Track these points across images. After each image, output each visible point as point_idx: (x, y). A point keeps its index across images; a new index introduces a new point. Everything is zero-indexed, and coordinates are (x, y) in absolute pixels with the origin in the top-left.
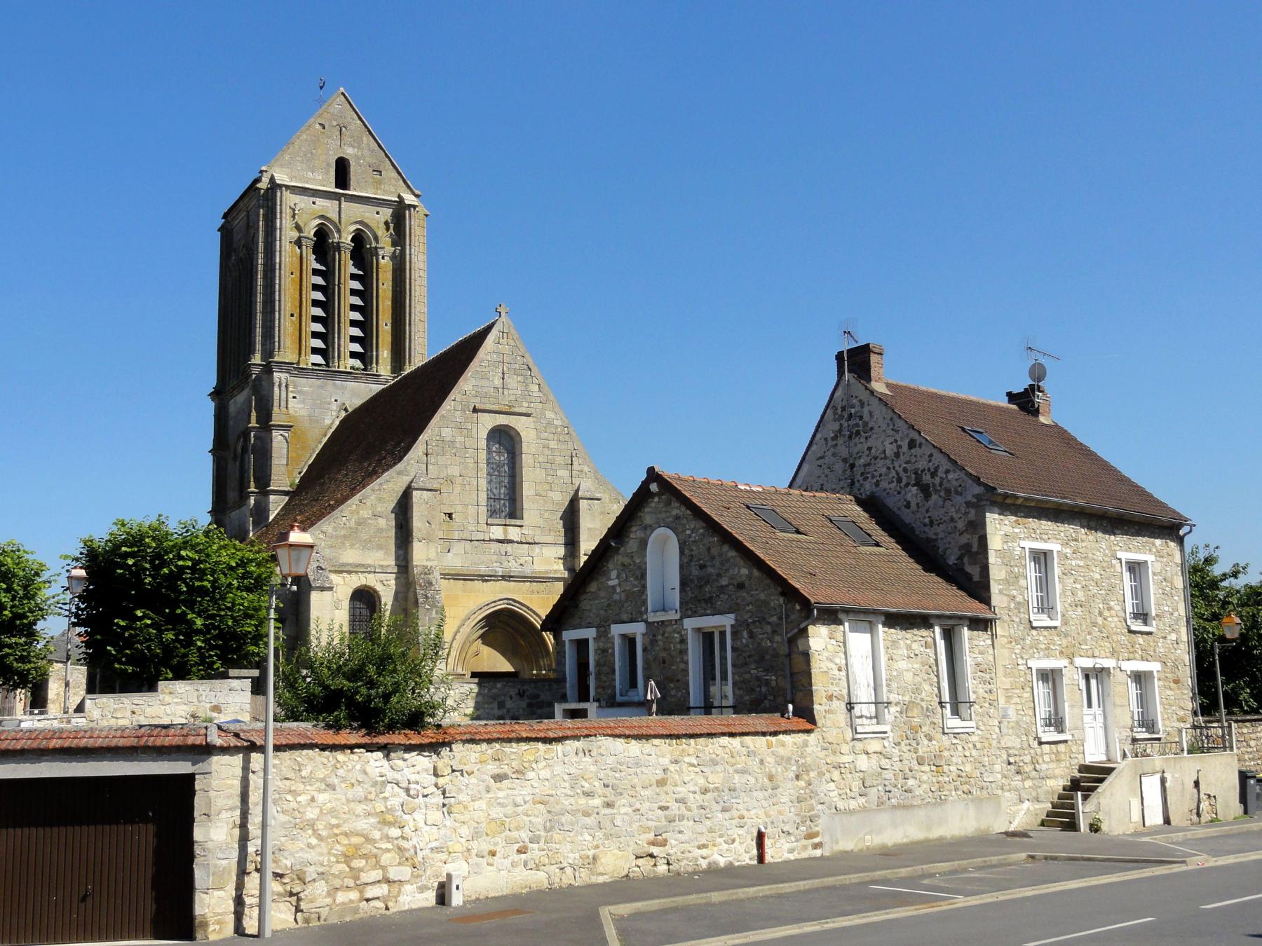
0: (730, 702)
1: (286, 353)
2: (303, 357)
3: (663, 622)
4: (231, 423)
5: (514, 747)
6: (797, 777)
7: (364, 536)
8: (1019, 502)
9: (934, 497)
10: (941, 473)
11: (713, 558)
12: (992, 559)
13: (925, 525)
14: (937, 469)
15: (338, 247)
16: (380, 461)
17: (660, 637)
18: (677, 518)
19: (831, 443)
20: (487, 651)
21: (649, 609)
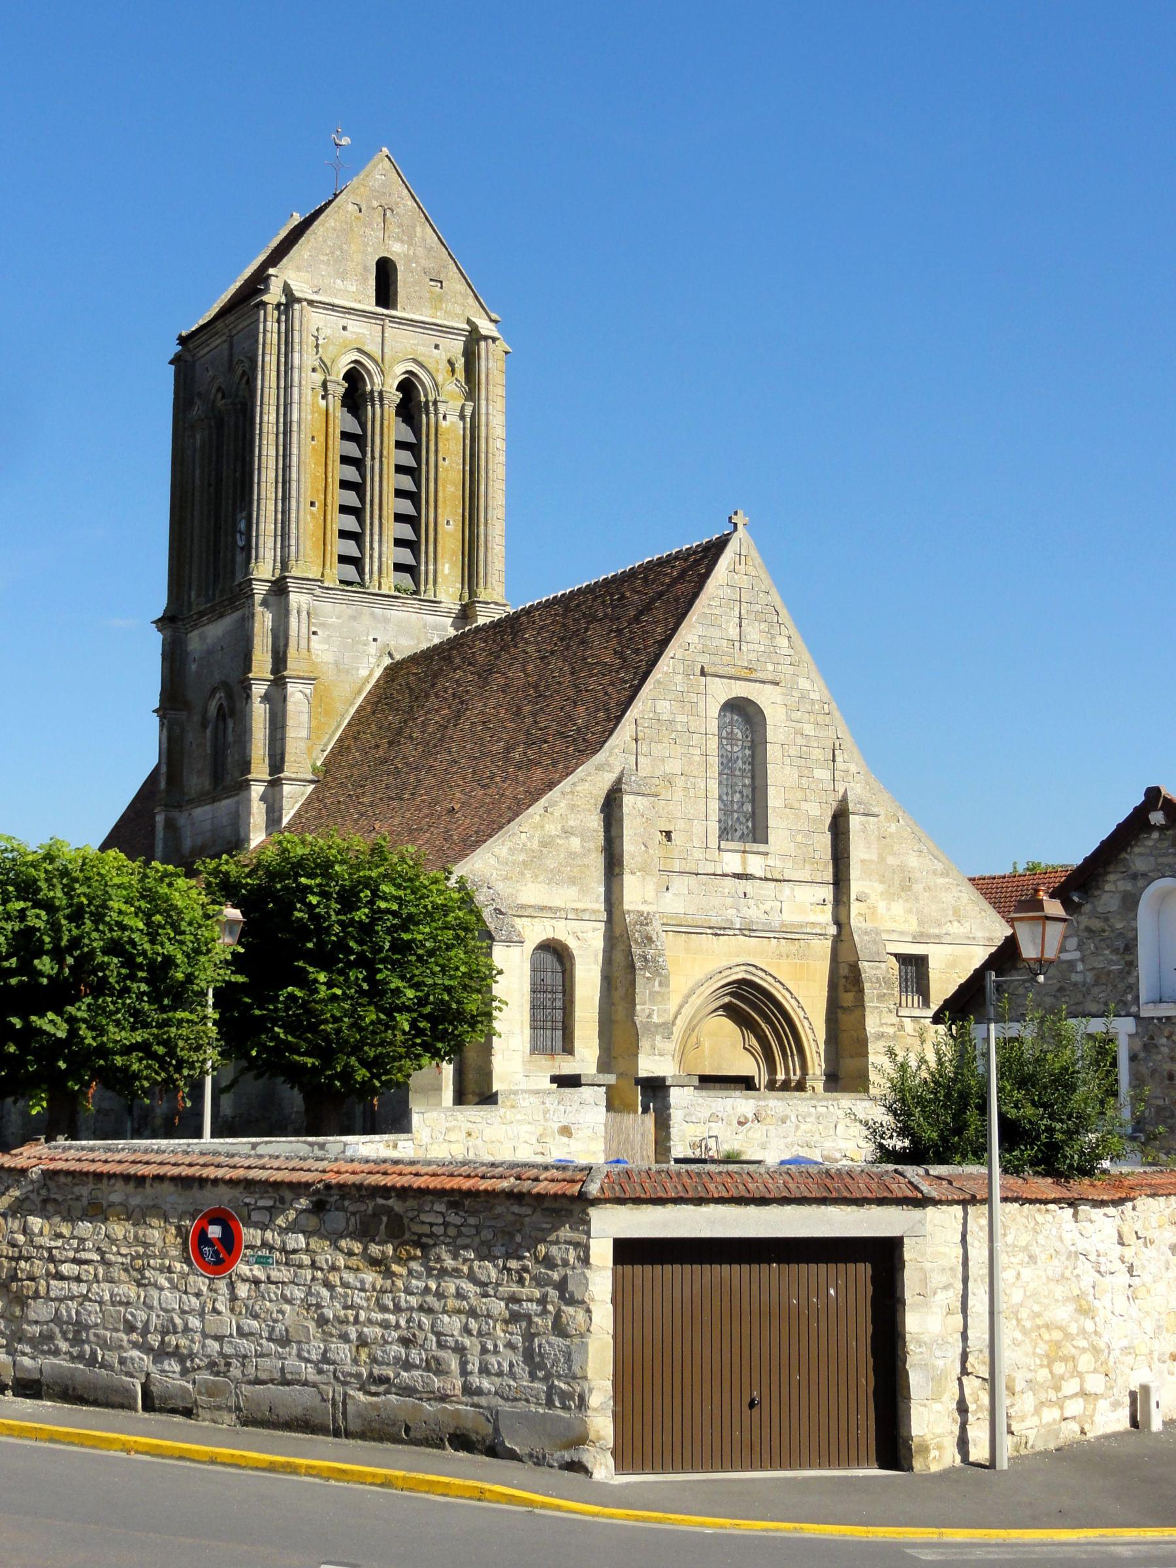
1: (305, 566)
3: (1168, 1018)
4: (194, 667)
7: (551, 864)
17: (1164, 1041)
21: (1142, 999)
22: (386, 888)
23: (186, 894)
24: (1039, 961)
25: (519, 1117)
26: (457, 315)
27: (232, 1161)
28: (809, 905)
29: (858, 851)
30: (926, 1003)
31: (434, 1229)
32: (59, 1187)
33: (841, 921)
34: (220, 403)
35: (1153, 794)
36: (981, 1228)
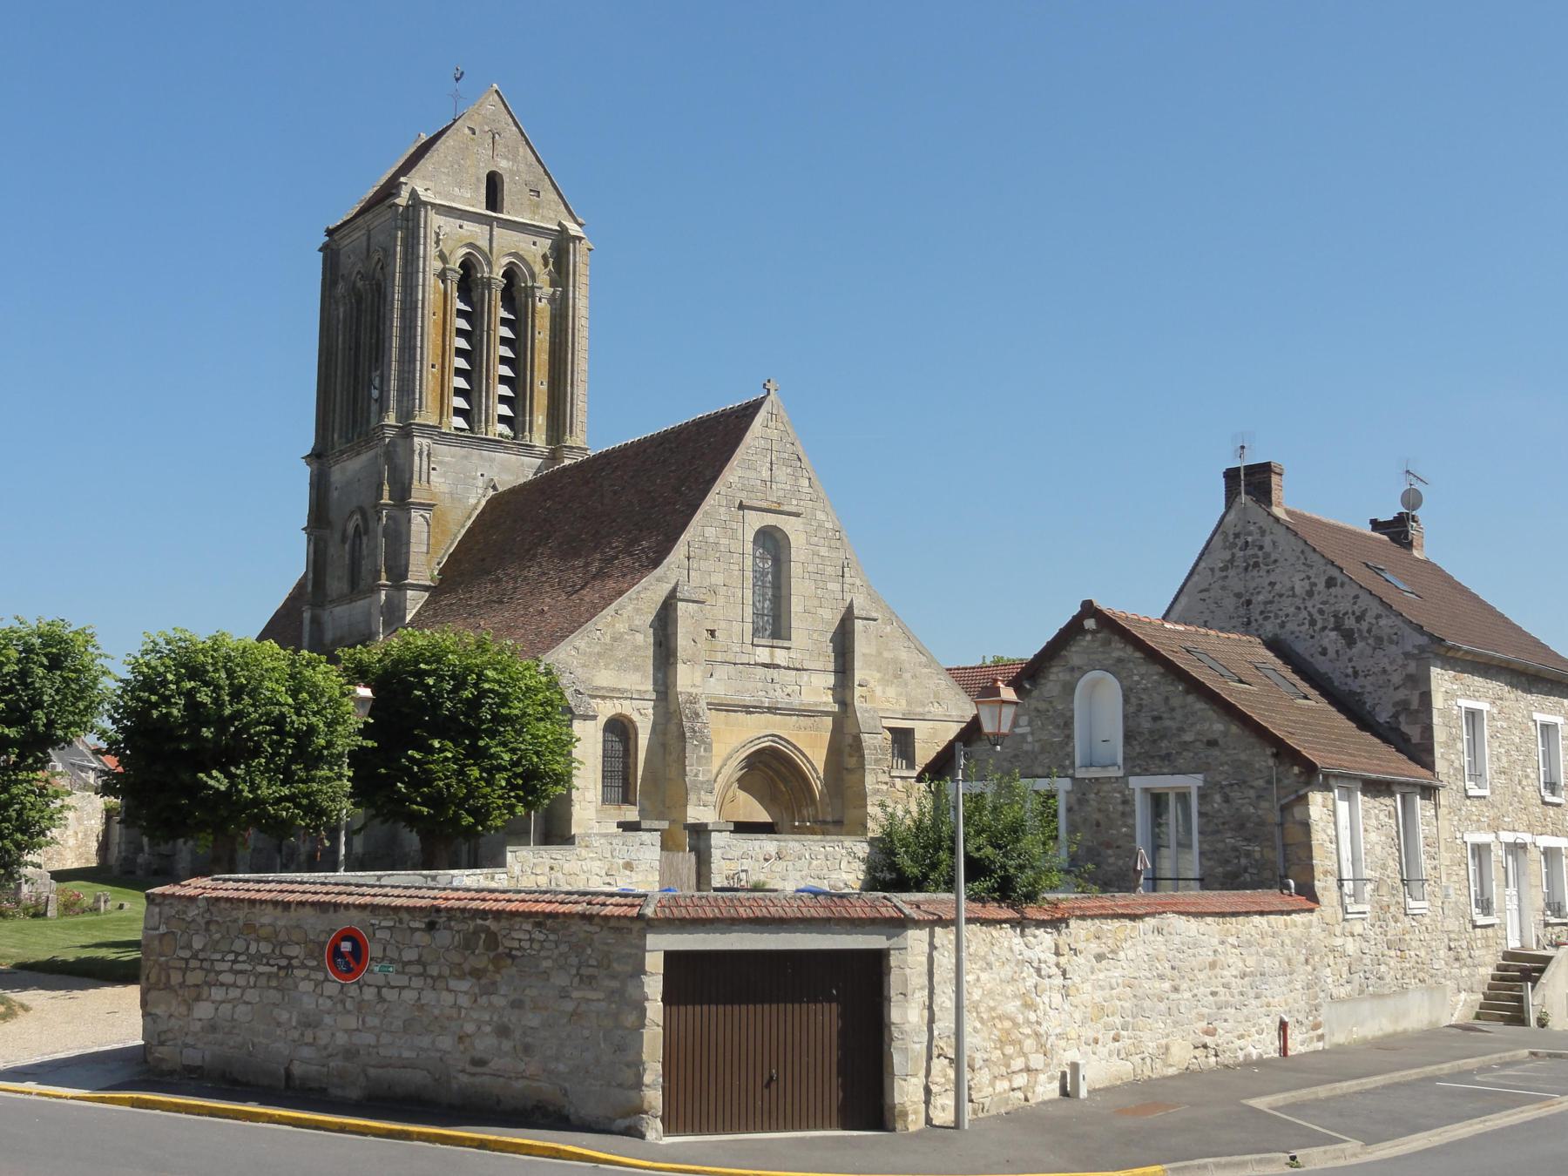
1: (427, 415)
3: (1097, 779)
4: (335, 494)
6: (1307, 961)
8: (1459, 654)
9: (1360, 645)
10: (1369, 618)
11: (1173, 709)
12: (1436, 720)
13: (1347, 676)
14: (1364, 613)
15: (488, 283)
16: (609, 561)
18: (1120, 660)
19: (1218, 574)
22: (490, 673)
23: (326, 676)
28: (818, 689)
30: (911, 765)
34: (360, 284)
35: (1088, 609)
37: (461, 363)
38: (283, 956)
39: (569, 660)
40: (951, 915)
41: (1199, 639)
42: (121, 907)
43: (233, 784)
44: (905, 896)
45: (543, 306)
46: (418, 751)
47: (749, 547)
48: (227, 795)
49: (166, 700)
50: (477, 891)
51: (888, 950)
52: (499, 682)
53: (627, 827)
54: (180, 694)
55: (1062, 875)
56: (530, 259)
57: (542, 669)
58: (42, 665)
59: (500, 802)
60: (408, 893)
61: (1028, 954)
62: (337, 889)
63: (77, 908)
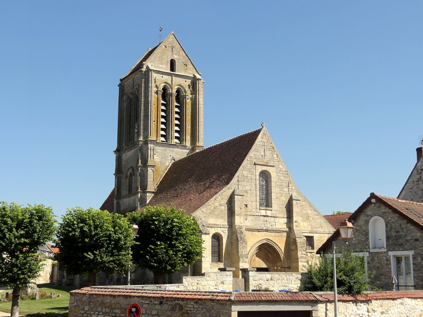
0: (413, 284)
1: (152, 137)
2: (158, 138)
3: (377, 252)
4: (124, 163)
5: (387, 302)
11: (403, 229)
15: (171, 95)
17: (376, 258)
18: (384, 213)
19: (416, 183)
20: (257, 259)
21: (371, 247)
22: (175, 220)
23: (124, 221)
24: (345, 239)
25: (211, 279)
26: (191, 73)
27: (138, 291)
28: (281, 223)
29: (296, 209)
30: (313, 248)
31: (191, 309)
32: (93, 298)
33: (290, 228)
34: (131, 96)
35: (373, 196)
36: (332, 308)
37: (163, 120)
38: (113, 313)
39: (200, 215)
40: (332, 299)
41: (410, 205)
42: (59, 296)
43: (95, 257)
44: (317, 293)
45: (189, 101)
46: (153, 245)
47: (258, 177)
48: (93, 260)
49: (74, 230)
50: (176, 291)
51: (312, 311)
52: (178, 223)
53: (221, 270)
54: (78, 228)
55: (369, 285)
56: (184, 86)
57: (192, 218)
58: (36, 219)
59: (179, 262)
60: (153, 292)
61: (358, 312)
62: (130, 291)
63: (45, 297)
